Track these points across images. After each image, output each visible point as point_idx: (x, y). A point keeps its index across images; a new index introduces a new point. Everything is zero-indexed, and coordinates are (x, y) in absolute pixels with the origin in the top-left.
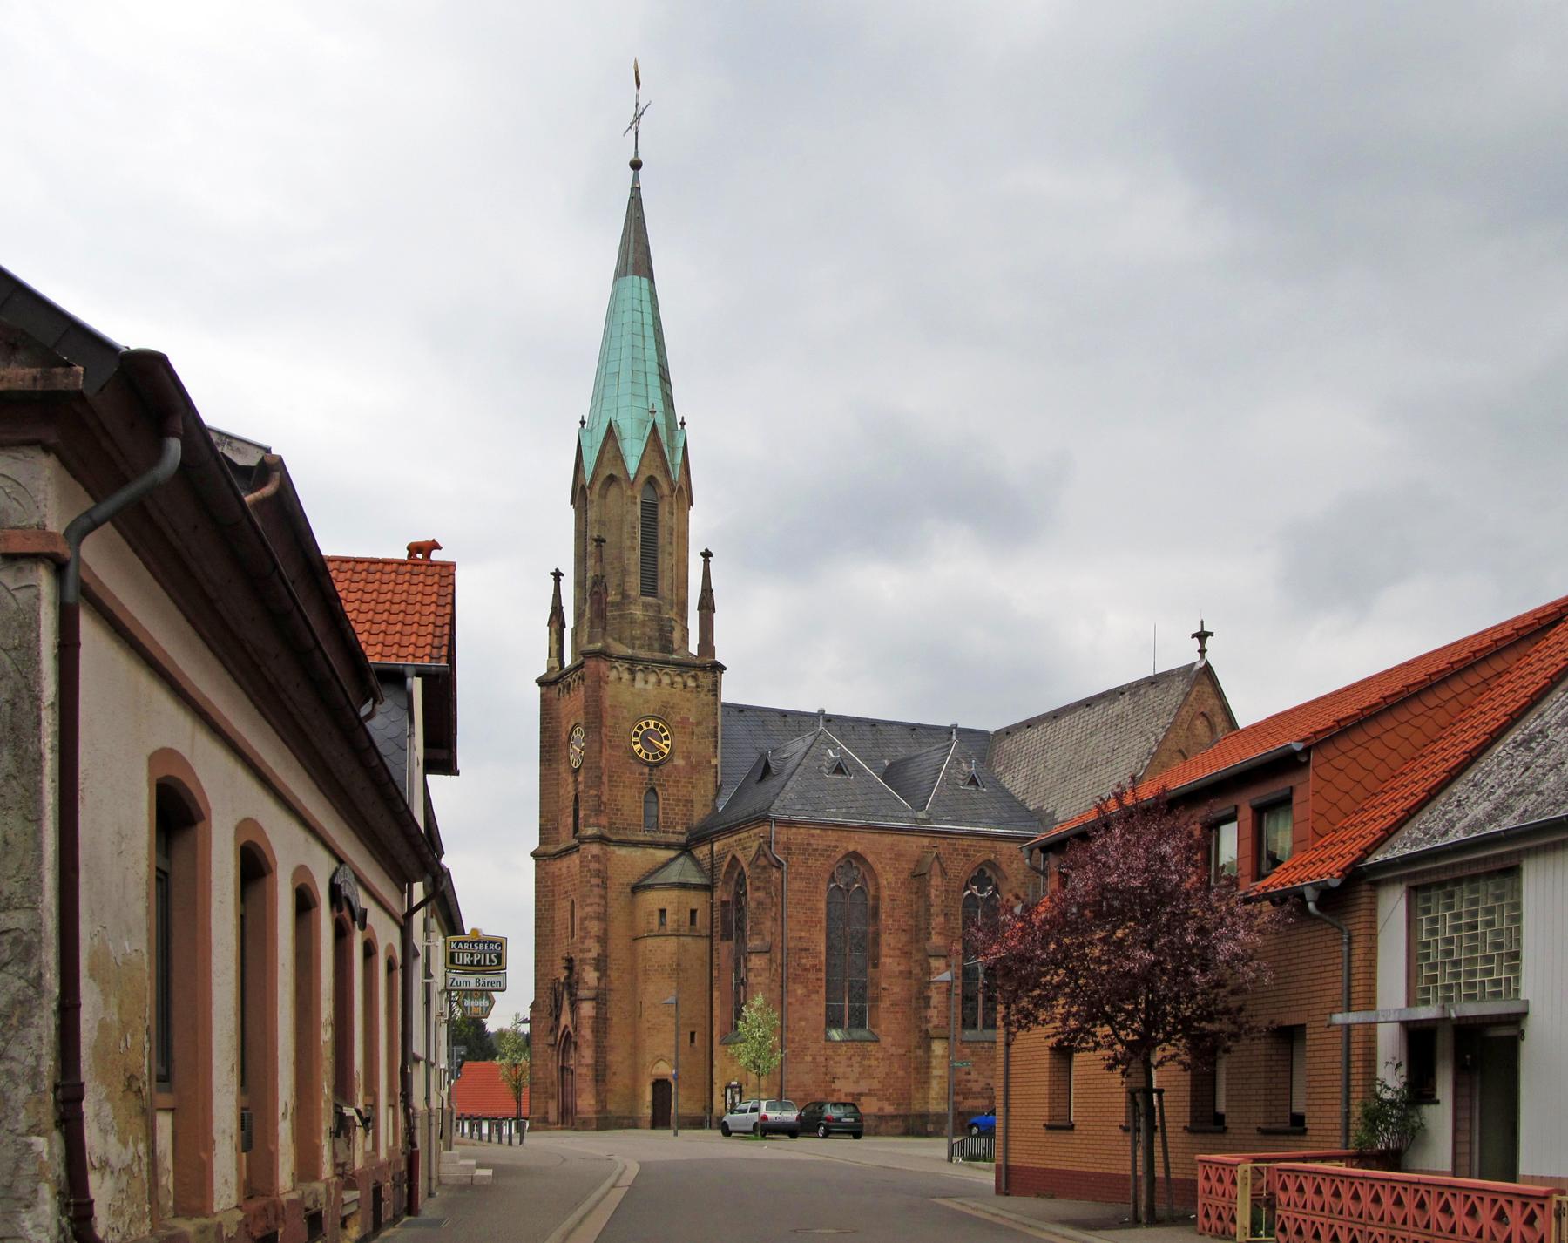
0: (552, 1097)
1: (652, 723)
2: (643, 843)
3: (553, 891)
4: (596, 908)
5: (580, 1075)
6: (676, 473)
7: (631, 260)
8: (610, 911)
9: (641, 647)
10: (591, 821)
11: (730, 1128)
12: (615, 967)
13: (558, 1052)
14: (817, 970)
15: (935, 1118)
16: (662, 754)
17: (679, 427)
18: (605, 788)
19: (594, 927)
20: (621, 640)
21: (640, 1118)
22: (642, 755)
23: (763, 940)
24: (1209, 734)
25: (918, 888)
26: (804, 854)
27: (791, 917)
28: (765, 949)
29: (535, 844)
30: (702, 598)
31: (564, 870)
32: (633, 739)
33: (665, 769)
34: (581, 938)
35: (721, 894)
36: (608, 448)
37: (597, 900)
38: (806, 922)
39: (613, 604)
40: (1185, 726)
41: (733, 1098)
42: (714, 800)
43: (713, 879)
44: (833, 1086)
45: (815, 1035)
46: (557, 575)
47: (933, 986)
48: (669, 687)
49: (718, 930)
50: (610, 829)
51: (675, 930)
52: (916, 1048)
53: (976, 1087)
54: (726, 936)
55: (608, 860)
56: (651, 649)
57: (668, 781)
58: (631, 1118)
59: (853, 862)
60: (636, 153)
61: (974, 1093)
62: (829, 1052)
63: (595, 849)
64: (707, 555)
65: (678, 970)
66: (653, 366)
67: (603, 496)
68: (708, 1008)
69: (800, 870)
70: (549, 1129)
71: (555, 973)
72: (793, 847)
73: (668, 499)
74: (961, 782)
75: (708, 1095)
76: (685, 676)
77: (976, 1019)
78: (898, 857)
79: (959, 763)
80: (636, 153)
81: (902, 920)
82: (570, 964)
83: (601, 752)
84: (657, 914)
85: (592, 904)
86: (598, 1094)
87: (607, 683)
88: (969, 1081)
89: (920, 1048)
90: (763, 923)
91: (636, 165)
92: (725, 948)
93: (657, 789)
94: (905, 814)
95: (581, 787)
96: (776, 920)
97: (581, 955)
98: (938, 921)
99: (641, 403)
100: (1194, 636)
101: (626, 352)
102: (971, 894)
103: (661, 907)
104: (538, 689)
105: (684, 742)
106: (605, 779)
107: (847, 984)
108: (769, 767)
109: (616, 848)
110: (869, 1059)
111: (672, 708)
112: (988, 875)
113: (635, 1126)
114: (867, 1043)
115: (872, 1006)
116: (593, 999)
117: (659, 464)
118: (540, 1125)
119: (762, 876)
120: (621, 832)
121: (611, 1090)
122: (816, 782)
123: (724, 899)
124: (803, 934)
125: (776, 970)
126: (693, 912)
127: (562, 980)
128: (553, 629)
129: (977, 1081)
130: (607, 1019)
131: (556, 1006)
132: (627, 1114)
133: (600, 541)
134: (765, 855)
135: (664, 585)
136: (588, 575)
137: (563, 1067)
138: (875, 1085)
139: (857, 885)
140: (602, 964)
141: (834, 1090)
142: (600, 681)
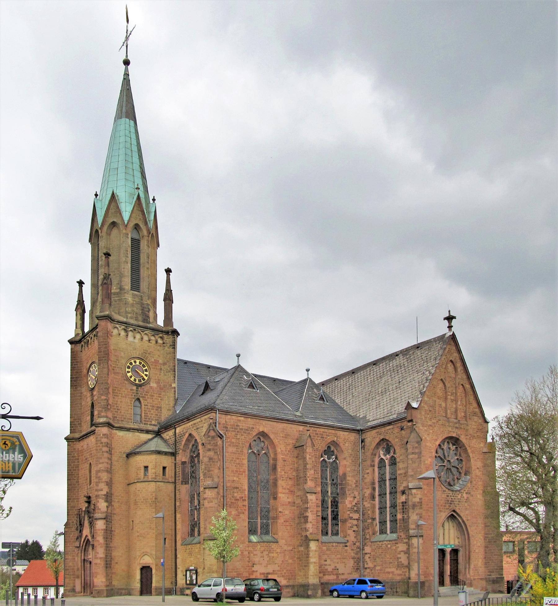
0: (78, 577)
1: (138, 361)
2: (133, 429)
3: (78, 459)
4: (105, 465)
5: (96, 564)
6: (151, 224)
7: (124, 110)
8: (113, 467)
9: (131, 318)
10: (103, 414)
11: (198, 596)
12: (116, 500)
13: (82, 551)
14: (243, 500)
15: (312, 587)
16: (144, 379)
17: (151, 202)
18: (110, 396)
19: (105, 476)
20: (119, 314)
21: (133, 589)
22: (132, 379)
23: (213, 480)
24: (454, 372)
25: (298, 454)
26: (235, 431)
27: (228, 468)
28: (214, 486)
29: (67, 433)
30: (166, 295)
31: (85, 447)
32: (127, 370)
33: (146, 388)
34: (96, 482)
35: (182, 457)
36: (112, 207)
37: (106, 460)
38: (237, 471)
39: (115, 294)
40: (444, 367)
41: (191, 577)
42: (174, 407)
43: (176, 449)
44: (254, 569)
45: (242, 538)
46: (81, 283)
47: (309, 510)
48: (147, 342)
49: (180, 479)
50: (114, 420)
51: (154, 478)
52: (298, 546)
53: (330, 569)
54: (185, 482)
55: (113, 438)
56: (137, 319)
57: (147, 395)
58: (127, 589)
59: (262, 438)
60: (127, 56)
61: (328, 572)
62: (251, 549)
63: (105, 430)
64: (168, 271)
65: (156, 503)
66: (137, 166)
67: (109, 234)
68: (173, 524)
69: (233, 440)
70: (76, 596)
71: (80, 505)
72: (229, 427)
73: (146, 238)
74: (315, 399)
75: (174, 575)
76: (157, 337)
77: (327, 530)
78: (287, 436)
79: (313, 389)
80: (127, 56)
81: (289, 472)
82: (89, 500)
83: (108, 375)
84: (143, 469)
85: (103, 463)
86: (107, 575)
87: (112, 336)
88: (326, 565)
89: (301, 546)
90: (213, 471)
91: (127, 63)
92: (184, 490)
93: (141, 399)
94: (289, 413)
95: (95, 398)
96: (220, 469)
97: (96, 493)
98: (310, 473)
99: (130, 184)
100: (445, 319)
101: (122, 157)
102: (324, 460)
103: (146, 465)
104: (69, 346)
105: (156, 374)
106: (111, 390)
107: (259, 509)
108: (208, 385)
109: (117, 431)
110: (273, 553)
111: (149, 354)
112: (332, 449)
113: (130, 594)
114: (272, 543)
115: (273, 522)
116: (104, 519)
117: (142, 218)
118: (70, 593)
119: (212, 442)
120: (120, 422)
121: (115, 573)
122: (238, 391)
123: (183, 460)
124: (235, 478)
125: (220, 499)
126: (164, 468)
127: (84, 509)
128: (78, 313)
129: (330, 565)
130: (112, 531)
131: (80, 524)
132: (124, 587)
133: (107, 255)
134: (214, 430)
135: (144, 285)
136: (100, 278)
137: (84, 560)
138: (277, 568)
139: (263, 452)
140: (109, 498)
141: (253, 571)
142: (108, 334)
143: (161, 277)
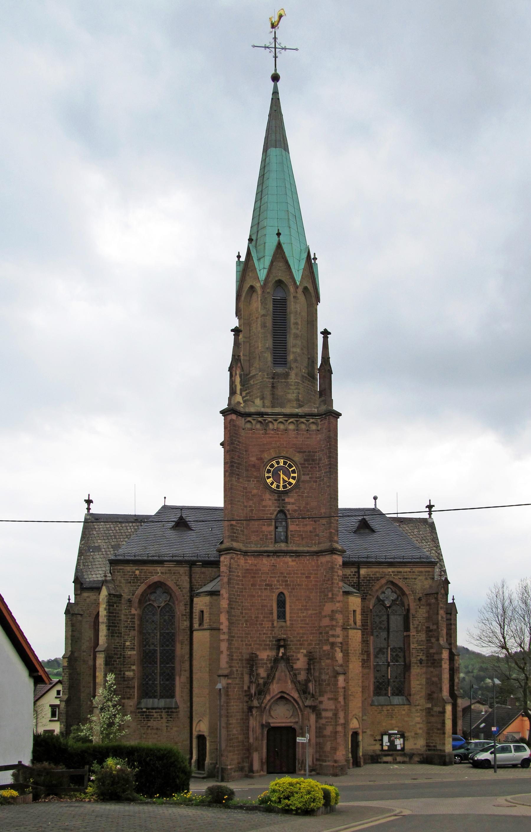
16: (290, 484)
60: (276, 70)
80: (276, 70)
91: (275, 78)
143: (320, 338)
